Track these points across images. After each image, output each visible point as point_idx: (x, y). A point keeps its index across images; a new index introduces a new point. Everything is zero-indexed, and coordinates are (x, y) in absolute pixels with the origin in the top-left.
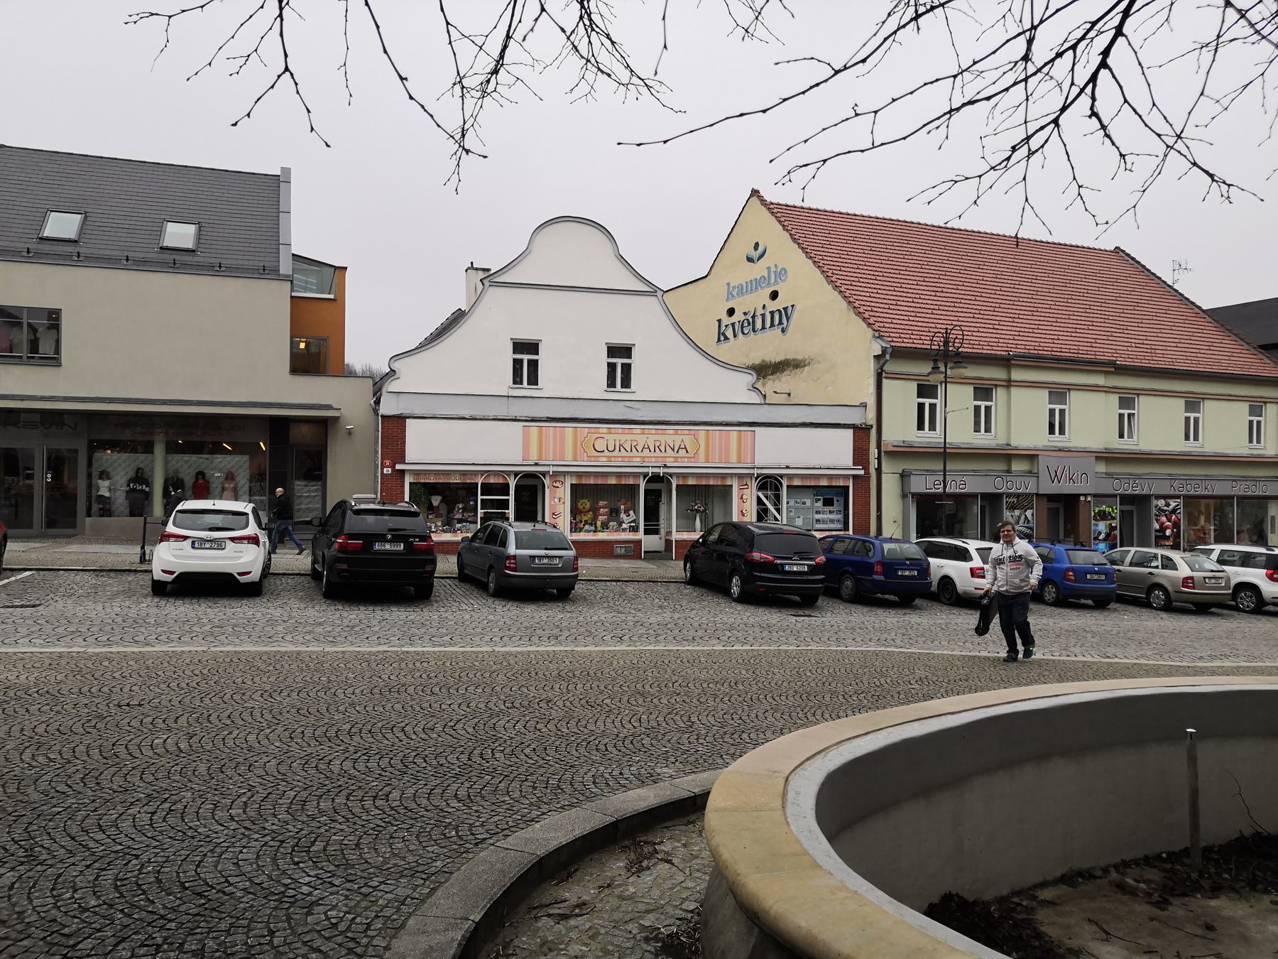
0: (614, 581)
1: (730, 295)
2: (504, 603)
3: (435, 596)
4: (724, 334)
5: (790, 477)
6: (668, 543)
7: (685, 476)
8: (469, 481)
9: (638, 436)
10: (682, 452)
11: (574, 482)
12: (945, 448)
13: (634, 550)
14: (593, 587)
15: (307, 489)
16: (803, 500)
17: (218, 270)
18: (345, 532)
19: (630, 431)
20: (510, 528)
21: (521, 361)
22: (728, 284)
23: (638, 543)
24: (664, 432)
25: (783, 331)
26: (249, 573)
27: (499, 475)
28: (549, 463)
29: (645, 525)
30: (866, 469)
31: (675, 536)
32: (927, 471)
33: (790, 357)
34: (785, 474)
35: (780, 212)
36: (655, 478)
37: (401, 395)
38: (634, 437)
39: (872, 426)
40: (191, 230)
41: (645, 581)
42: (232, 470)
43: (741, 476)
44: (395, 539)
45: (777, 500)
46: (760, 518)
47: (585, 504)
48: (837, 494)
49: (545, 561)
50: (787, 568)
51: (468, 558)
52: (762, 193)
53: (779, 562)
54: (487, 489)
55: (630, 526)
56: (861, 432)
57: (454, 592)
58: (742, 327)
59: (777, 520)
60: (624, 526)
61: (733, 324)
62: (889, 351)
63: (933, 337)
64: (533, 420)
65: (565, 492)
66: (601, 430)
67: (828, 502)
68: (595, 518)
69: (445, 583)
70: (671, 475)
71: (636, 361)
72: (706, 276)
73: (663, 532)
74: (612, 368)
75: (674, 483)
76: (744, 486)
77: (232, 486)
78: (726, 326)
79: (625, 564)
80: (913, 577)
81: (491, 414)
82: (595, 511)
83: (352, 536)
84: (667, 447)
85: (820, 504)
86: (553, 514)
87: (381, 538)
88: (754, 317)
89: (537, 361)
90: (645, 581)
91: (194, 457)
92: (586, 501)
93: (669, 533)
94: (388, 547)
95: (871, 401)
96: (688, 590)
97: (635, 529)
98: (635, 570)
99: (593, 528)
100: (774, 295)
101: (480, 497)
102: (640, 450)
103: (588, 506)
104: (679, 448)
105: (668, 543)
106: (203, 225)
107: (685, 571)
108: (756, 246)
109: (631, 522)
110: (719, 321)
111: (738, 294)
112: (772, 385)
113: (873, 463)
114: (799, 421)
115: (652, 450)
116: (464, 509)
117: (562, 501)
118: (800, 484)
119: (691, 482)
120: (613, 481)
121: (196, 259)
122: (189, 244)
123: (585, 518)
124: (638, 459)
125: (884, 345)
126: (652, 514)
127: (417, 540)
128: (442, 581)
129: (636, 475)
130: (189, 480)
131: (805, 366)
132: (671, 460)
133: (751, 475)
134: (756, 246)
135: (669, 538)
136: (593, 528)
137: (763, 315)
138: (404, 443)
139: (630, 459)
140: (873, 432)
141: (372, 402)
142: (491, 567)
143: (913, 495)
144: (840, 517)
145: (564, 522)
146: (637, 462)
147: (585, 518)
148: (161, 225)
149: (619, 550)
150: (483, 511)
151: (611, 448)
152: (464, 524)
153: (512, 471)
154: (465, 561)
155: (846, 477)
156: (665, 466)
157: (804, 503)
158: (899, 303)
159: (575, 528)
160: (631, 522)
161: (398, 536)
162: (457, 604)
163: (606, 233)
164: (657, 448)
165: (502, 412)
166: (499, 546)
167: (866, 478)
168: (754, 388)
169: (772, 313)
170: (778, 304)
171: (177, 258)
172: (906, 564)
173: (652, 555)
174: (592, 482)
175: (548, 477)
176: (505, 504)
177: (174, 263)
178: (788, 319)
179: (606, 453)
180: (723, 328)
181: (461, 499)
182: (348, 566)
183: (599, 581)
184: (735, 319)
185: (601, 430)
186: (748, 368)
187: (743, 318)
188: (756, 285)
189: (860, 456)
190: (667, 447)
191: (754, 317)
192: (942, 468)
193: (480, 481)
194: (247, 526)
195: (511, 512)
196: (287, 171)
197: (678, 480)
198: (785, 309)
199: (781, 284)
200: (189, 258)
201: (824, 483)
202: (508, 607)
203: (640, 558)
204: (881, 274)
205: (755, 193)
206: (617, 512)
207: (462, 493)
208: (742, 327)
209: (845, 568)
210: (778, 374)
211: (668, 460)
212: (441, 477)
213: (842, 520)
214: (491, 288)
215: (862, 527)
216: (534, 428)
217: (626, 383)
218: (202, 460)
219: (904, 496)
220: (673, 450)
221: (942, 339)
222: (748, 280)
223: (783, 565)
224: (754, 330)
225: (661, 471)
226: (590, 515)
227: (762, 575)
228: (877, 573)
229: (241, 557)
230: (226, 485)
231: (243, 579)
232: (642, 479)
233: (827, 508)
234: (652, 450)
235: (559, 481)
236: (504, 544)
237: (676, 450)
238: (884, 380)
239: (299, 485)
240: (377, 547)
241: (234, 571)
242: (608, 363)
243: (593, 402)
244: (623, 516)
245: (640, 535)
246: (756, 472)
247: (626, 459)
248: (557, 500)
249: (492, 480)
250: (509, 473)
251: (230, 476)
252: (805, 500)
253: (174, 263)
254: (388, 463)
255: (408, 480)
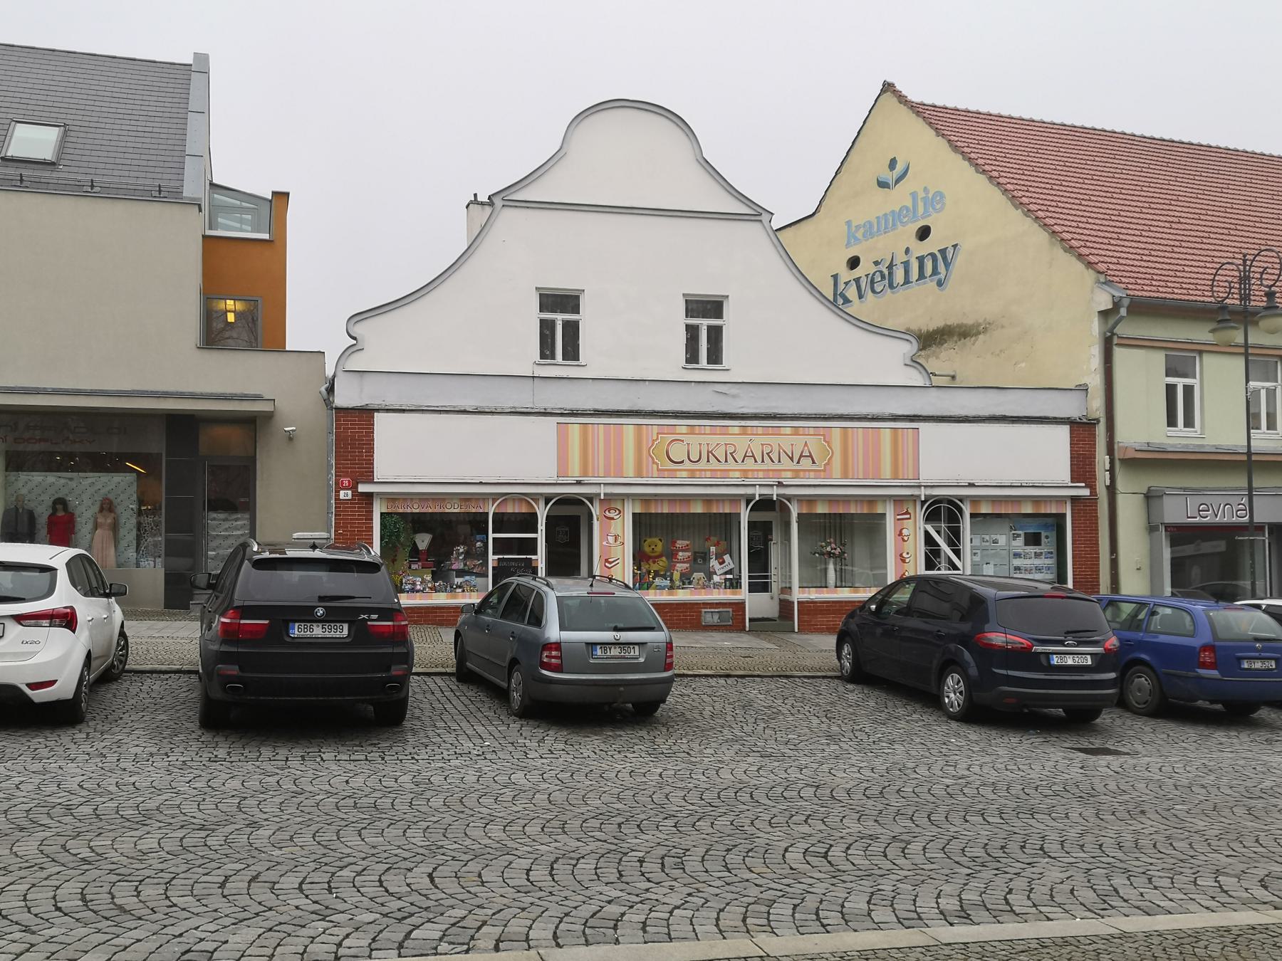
0: (721, 676)
1: (851, 239)
2: (540, 732)
3: (413, 717)
4: (842, 295)
5: (975, 500)
6: (786, 607)
7: (811, 500)
8: (474, 511)
9: (735, 438)
10: (806, 463)
11: (638, 511)
12: (1249, 453)
13: (734, 619)
14: (688, 691)
15: (227, 525)
16: (994, 537)
17: (88, 190)
18: (236, 604)
19: (724, 431)
20: (546, 589)
21: (553, 322)
22: (849, 223)
23: (739, 606)
24: (776, 432)
25: (940, 284)
26: (51, 683)
27: (521, 500)
28: (599, 483)
29: (750, 577)
30: (1091, 486)
31: (798, 595)
32: (1185, 489)
33: (953, 321)
34: (968, 496)
35: (931, 115)
36: (765, 504)
37: (367, 377)
38: (728, 439)
39: (1098, 421)
40: (52, 135)
41: (772, 677)
42: (111, 497)
43: (898, 500)
44: (333, 616)
45: (954, 539)
46: (930, 565)
47: (655, 544)
48: (1046, 527)
49: (615, 652)
50: (1055, 660)
51: (470, 637)
52: (898, 87)
53: (1039, 649)
54: (502, 522)
55: (726, 579)
56: (1081, 430)
57: (448, 706)
58: (872, 282)
59: (956, 568)
60: (716, 579)
61: (857, 280)
62: (1126, 302)
63: (1215, 275)
64: (573, 414)
65: (624, 527)
66: (678, 429)
67: (1033, 540)
68: (671, 568)
69: (432, 686)
70: (789, 498)
71: (730, 322)
72: (814, 214)
73: (775, 587)
74: (692, 332)
75: (795, 511)
76: (903, 515)
77: (109, 521)
78: (846, 283)
79: (726, 641)
80: (1266, 672)
81: (508, 404)
82: (671, 555)
83: (246, 611)
84: (783, 454)
85: (1020, 542)
86: (607, 561)
87: (305, 614)
88: (890, 267)
89: (1169, 373)
90: (772, 677)
91: (51, 478)
92: (656, 540)
93: (787, 589)
94: (318, 631)
95: (1095, 381)
96: (854, 694)
97: (734, 584)
98: (747, 653)
99: (668, 583)
100: (924, 233)
101: (491, 536)
102: (740, 461)
103: (659, 547)
104: (801, 456)
105: (786, 607)
106: (71, 128)
107: (839, 657)
108: (893, 164)
109: (726, 573)
110: (835, 277)
111: (864, 236)
112: (945, 360)
113: (1103, 478)
114: (986, 414)
115: (759, 459)
116: (468, 555)
117: (620, 540)
118: (990, 512)
119: (821, 509)
120: (698, 509)
121: (55, 175)
122: (48, 154)
123: (654, 567)
124: (737, 474)
125: (1117, 294)
126: (759, 559)
127: (375, 617)
128: (426, 679)
129: (734, 499)
130: (43, 512)
131: (979, 333)
132: (789, 474)
133: (914, 499)
134: (893, 164)
135: (787, 597)
136: (668, 583)
137: (906, 265)
138: (371, 450)
139: (724, 474)
140: (1101, 430)
141: (323, 389)
142: (514, 662)
143: (1168, 527)
144: (1051, 562)
145: (625, 570)
146: (735, 478)
147: (654, 567)
148: (6, 127)
149: (709, 618)
150: (496, 557)
151: (695, 457)
152: (467, 578)
153: (541, 494)
154: (468, 648)
155: (1060, 500)
156: (780, 485)
157: (995, 542)
158: (1121, 236)
159: (642, 582)
160: (726, 573)
161: (337, 611)
162: (450, 738)
163: (687, 130)
164: (766, 457)
165: (524, 402)
166: (529, 623)
167: (1091, 502)
168: (914, 362)
169: (921, 260)
170: (931, 245)
171: (25, 173)
172: (1256, 650)
173: (761, 626)
174: (666, 511)
175: (597, 504)
176: (530, 546)
177: (21, 180)
178: (947, 265)
179: (688, 465)
180: (841, 286)
181: (462, 538)
182: (241, 669)
183: (695, 676)
184: (858, 272)
185: (678, 429)
186: (908, 332)
187: (873, 269)
188: (890, 222)
189: (1082, 467)
190: (783, 454)
191: (890, 267)
192: (1246, 485)
193: (491, 510)
194: (50, 591)
195: (540, 559)
196: (202, 59)
197: (800, 507)
198: (943, 252)
199: (934, 215)
200: (45, 174)
201: (1028, 509)
202: (549, 740)
203: (742, 629)
204: (1087, 197)
205: (888, 87)
206: (705, 557)
207: (464, 530)
208: (872, 282)
209: (1132, 656)
210: (934, 348)
211: (784, 474)
212: (430, 503)
213: (1054, 566)
214: (505, 209)
215: (1088, 581)
216: (574, 428)
217: (715, 356)
218: (63, 481)
219: (1152, 529)
220: (792, 459)
221: (1237, 274)
222: (881, 214)
223: (1048, 655)
224: (891, 286)
225: (775, 492)
226: (663, 562)
227: (1011, 673)
228: (1204, 665)
229: (35, 653)
230: (100, 520)
231: (38, 696)
232: (743, 505)
233: (1032, 550)
234: (759, 460)
235: (615, 509)
236: (537, 619)
237: (796, 459)
238: (1115, 347)
239: (214, 519)
240: (297, 631)
241: (20, 681)
242: (687, 326)
243: (666, 385)
244: (714, 563)
245: (743, 594)
246: (923, 493)
247: (719, 474)
248: (611, 539)
249: (510, 509)
250: (535, 497)
251: (107, 506)
252: (998, 537)
253: (21, 180)
254: (346, 483)
255: (378, 509)
